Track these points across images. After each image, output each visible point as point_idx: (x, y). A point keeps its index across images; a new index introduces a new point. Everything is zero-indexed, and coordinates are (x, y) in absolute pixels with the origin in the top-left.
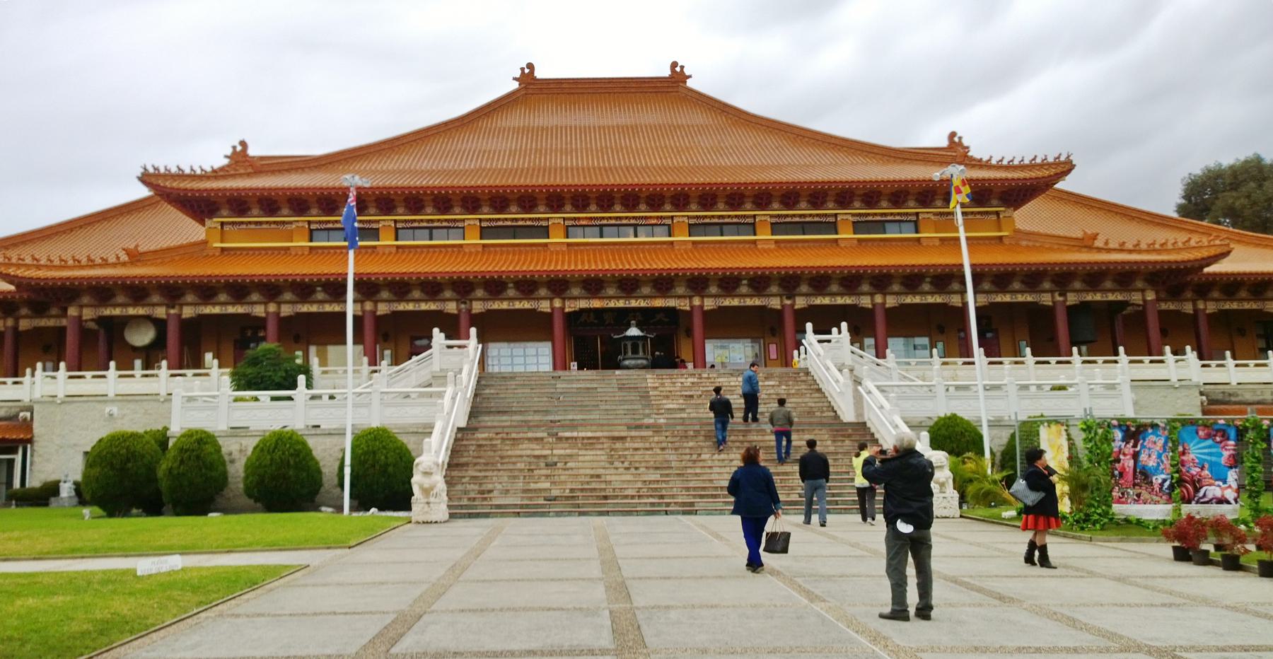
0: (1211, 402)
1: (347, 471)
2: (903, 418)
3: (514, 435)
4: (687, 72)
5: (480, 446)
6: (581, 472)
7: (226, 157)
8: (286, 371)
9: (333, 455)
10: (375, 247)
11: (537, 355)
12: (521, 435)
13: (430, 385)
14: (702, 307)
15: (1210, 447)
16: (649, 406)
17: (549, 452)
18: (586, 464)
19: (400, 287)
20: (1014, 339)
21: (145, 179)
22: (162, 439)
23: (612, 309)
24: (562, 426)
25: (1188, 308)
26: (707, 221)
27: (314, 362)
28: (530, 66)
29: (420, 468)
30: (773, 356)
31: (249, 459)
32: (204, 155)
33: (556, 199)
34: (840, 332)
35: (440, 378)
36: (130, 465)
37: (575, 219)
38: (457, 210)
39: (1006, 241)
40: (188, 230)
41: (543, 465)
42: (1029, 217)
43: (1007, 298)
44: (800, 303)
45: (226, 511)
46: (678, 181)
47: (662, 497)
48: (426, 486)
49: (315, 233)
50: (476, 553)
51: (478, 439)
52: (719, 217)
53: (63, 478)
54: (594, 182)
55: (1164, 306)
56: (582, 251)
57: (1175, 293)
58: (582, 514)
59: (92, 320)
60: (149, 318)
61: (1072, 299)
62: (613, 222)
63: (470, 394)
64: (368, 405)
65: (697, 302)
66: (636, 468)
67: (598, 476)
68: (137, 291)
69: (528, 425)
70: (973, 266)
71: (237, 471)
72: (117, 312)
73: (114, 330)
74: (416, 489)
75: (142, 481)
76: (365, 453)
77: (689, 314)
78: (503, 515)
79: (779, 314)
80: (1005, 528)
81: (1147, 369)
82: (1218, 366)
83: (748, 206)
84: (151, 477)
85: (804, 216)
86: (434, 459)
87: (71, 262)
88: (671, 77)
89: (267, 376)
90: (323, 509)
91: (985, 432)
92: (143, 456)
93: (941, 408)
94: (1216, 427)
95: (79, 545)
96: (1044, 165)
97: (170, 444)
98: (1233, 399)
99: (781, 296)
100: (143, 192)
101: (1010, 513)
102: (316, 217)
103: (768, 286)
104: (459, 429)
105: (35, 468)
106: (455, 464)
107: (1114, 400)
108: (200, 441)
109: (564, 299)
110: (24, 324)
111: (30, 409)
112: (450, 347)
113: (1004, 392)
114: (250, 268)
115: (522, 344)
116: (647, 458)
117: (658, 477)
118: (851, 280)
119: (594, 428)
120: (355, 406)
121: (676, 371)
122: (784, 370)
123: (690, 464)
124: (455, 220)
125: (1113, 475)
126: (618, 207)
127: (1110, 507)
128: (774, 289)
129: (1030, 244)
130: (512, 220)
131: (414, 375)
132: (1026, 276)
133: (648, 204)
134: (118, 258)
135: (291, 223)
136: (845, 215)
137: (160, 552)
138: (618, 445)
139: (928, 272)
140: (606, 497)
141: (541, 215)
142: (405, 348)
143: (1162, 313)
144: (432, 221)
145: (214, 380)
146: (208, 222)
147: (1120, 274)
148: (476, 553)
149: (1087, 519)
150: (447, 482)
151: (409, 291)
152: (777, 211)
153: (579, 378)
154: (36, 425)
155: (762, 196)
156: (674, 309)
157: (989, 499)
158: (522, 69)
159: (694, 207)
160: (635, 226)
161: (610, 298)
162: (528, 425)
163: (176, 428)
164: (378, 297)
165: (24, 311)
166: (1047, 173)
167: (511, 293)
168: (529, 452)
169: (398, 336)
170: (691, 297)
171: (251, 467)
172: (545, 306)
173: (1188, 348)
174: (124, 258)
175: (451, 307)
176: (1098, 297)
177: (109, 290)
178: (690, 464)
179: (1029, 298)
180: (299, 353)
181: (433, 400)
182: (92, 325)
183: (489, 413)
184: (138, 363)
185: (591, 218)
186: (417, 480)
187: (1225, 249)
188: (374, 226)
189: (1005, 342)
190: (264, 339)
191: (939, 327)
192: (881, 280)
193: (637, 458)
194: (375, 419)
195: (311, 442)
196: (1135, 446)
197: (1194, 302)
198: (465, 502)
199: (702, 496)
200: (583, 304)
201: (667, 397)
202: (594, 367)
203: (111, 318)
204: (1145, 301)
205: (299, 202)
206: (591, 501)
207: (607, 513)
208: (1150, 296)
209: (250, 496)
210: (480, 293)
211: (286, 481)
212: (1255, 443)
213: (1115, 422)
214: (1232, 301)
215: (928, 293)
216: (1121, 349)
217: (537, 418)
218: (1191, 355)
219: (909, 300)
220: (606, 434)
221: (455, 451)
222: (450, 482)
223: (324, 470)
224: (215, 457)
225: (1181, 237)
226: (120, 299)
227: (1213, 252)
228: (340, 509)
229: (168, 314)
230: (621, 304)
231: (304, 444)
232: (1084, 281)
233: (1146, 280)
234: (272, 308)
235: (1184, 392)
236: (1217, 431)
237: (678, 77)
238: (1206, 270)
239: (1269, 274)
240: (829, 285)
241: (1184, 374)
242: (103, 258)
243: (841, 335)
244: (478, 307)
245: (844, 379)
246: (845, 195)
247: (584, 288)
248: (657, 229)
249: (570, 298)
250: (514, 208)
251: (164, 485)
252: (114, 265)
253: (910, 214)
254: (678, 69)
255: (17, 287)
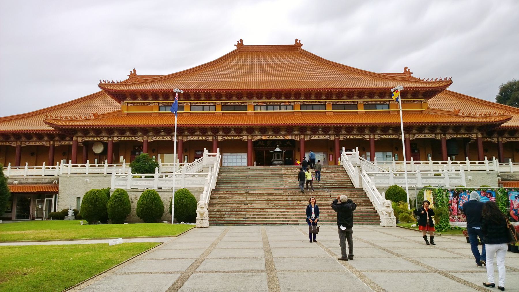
0: (503, 180)
1: (173, 206)
2: (376, 186)
3: (232, 192)
4: (302, 43)
5: (220, 196)
6: (257, 207)
7: (128, 76)
8: (150, 165)
9: (167, 199)
10: (182, 113)
11: (237, 159)
12: (235, 192)
13: (202, 171)
14: (304, 139)
15: (485, 199)
16: (282, 181)
17: (245, 199)
18: (259, 204)
19: (192, 130)
20: (426, 152)
21: (100, 85)
22: (108, 192)
23: (279, 140)
24: (250, 189)
25: (495, 141)
26: (308, 103)
27: (160, 161)
28: (241, 40)
29: (200, 205)
30: (331, 160)
31: (138, 201)
32: (118, 75)
33: (250, 94)
34: (355, 151)
35: (205, 169)
36: (97, 203)
37: (257, 102)
38: (213, 99)
39: (424, 113)
40: (115, 106)
41: (243, 204)
42: (433, 103)
43: (423, 136)
44: (342, 138)
45: (130, 222)
46: (297, 88)
47: (286, 218)
48: (201, 213)
49: (161, 108)
50: (220, 239)
51: (219, 194)
52: (312, 102)
53: (70, 208)
54: (265, 88)
55: (485, 140)
56: (269, 116)
57: (490, 135)
58: (257, 224)
59: (81, 142)
60: (101, 142)
61: (448, 137)
62: (272, 104)
63: (216, 175)
64: (180, 180)
65: (302, 137)
66: (277, 206)
67: (263, 209)
68: (98, 131)
69: (237, 188)
70: (404, 123)
71: (134, 205)
72: (90, 139)
73: (89, 145)
74: (198, 214)
75: (103, 210)
76: (179, 199)
77: (299, 142)
78: (229, 225)
79: (333, 142)
80: (412, 231)
81: (477, 166)
82: (506, 165)
83: (323, 98)
84: (105, 209)
85: (345, 102)
86: (204, 202)
87: (74, 119)
88: (295, 45)
89: (145, 168)
90: (164, 221)
91: (407, 192)
92: (102, 200)
93: (391, 182)
94: (488, 192)
95: (84, 235)
96: (441, 81)
97: (111, 195)
98: (511, 178)
99: (334, 135)
100: (100, 90)
101: (414, 225)
102: (161, 101)
103: (329, 131)
104: (213, 190)
105: (60, 203)
106: (211, 204)
107: (458, 180)
108: (121, 194)
109: (252, 136)
110: (57, 144)
111: (58, 180)
112: (209, 156)
113: (423, 177)
114: (138, 123)
115: (236, 154)
116: (281, 202)
117: (284, 210)
118: (362, 129)
119: (262, 190)
120: (176, 180)
121: (293, 166)
122: (334, 166)
123: (297, 205)
124: (212, 103)
125: (449, 210)
126: (273, 98)
127: (449, 222)
128: (332, 132)
129: (433, 114)
130: (234, 103)
131: (196, 167)
132: (430, 127)
133: (285, 97)
134: (90, 117)
135: (152, 103)
136: (361, 102)
137: (114, 237)
138: (270, 197)
139: (391, 125)
140: (266, 218)
141: (244, 101)
142: (192, 156)
143: (484, 143)
144: (204, 103)
145: (124, 168)
146: (122, 103)
147: (442, 127)
148: (220, 239)
149: (440, 227)
150: (209, 211)
151: (195, 132)
152: (334, 100)
153: (257, 169)
154: (60, 186)
155: (329, 94)
156: (293, 140)
157: (407, 219)
158: (238, 42)
159: (302, 98)
160: (280, 105)
161: (269, 135)
162: (237, 188)
163: (113, 188)
164: (184, 134)
165: (57, 138)
166: (441, 85)
167: (233, 133)
168: (238, 199)
169: (191, 151)
170: (300, 135)
171: (139, 204)
172: (245, 138)
173: (494, 158)
174: (93, 117)
175: (210, 139)
176: (459, 136)
177: (87, 130)
178: (297, 205)
179: (431, 136)
180: (154, 157)
181: (203, 178)
182: (81, 145)
183: (223, 183)
184: (96, 160)
185: (263, 102)
186: (198, 210)
187: (509, 117)
188: (183, 105)
189: (422, 155)
190: (142, 151)
191: (391, 147)
192: (373, 129)
193: (277, 202)
194: (183, 184)
195: (160, 194)
196: (457, 199)
197: (498, 138)
198: (215, 219)
199: (301, 218)
200: (259, 138)
201: (289, 177)
202: (262, 164)
203: (88, 141)
204: (477, 138)
205: (155, 95)
206: (260, 219)
207: (266, 224)
208: (480, 136)
209: (139, 216)
210: (221, 133)
211: (151, 211)
212: (502, 198)
213: (449, 189)
214: (513, 138)
215: (463, 133)
216: (467, 158)
217: (241, 185)
218: (495, 161)
219: (384, 137)
220: (266, 192)
221: (211, 199)
222: (209, 212)
223: (164, 206)
224: (127, 200)
225: (498, 112)
226: (92, 134)
227: (504, 118)
228: (170, 222)
229: (108, 140)
230: (273, 138)
231: (158, 195)
232: (453, 130)
233: (478, 129)
234: (145, 138)
235: (492, 176)
236: (488, 193)
237: (298, 45)
238: (502, 125)
239: (518, 127)
240: (353, 131)
241: (492, 168)
242: (83, 117)
243: (356, 152)
244: (220, 139)
245: (355, 170)
246: (361, 93)
247: (260, 131)
248: (262, 107)
249: (254, 135)
250: (234, 98)
251: (109, 211)
252: (89, 120)
253: (386, 101)
254: (298, 42)
255: (55, 128)
